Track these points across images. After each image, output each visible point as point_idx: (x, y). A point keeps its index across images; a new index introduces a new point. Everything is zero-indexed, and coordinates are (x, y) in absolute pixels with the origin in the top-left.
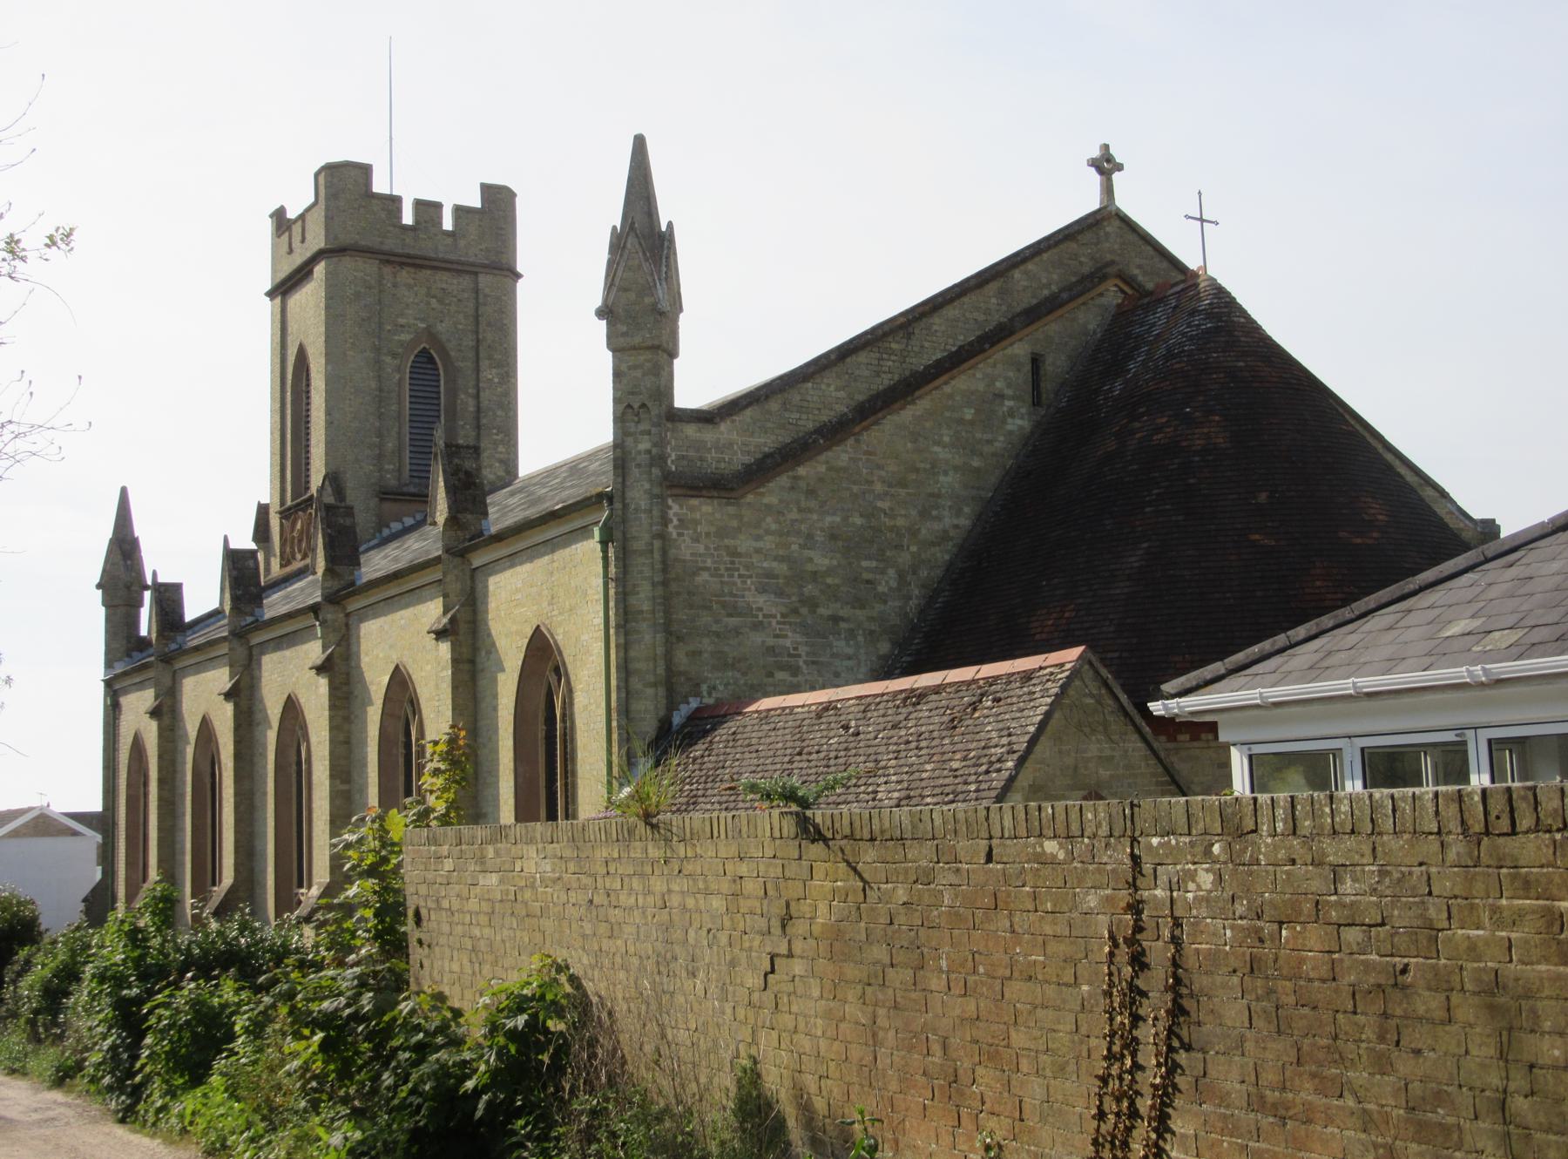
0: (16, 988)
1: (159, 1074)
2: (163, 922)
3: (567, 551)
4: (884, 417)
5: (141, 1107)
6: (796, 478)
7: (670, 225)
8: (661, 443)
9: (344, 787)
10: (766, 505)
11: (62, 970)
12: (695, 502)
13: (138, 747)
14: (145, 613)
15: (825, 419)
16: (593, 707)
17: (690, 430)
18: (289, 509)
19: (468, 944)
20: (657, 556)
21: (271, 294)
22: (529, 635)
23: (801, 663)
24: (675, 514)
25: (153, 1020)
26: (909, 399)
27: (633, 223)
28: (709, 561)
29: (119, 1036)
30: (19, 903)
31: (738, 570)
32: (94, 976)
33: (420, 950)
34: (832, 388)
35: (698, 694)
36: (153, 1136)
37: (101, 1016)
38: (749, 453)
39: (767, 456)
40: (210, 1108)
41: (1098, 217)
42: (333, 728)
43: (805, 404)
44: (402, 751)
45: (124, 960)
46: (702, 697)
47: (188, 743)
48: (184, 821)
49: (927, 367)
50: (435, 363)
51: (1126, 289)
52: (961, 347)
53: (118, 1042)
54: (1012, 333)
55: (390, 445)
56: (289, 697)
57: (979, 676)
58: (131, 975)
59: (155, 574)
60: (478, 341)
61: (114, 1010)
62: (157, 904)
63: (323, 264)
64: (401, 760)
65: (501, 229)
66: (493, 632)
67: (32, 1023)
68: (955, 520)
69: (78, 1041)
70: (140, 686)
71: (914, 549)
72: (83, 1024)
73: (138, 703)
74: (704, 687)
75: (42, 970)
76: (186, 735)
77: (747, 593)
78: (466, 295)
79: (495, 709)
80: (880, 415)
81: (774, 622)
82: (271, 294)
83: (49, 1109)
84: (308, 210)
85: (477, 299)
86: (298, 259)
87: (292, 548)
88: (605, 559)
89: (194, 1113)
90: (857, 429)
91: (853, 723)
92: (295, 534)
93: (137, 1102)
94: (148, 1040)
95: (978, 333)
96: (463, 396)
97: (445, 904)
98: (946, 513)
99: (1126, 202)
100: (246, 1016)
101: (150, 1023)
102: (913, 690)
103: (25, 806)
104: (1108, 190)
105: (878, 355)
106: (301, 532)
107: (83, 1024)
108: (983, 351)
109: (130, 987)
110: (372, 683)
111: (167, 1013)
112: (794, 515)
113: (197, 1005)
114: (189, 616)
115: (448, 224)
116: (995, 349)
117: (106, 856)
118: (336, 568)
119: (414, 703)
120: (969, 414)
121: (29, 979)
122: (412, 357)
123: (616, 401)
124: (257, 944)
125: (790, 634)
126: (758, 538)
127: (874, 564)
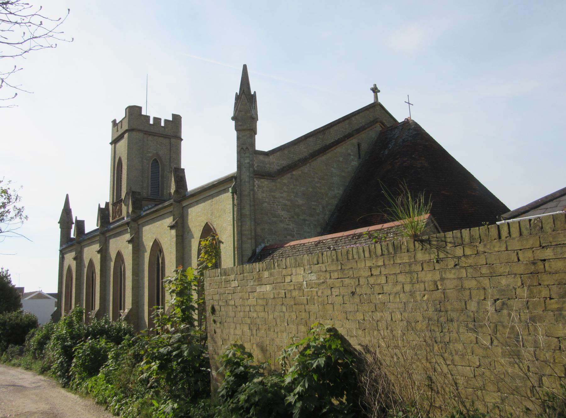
0: (29, 342)
1: (77, 372)
2: (80, 320)
3: (218, 198)
4: (318, 158)
5: (71, 383)
6: (293, 175)
7: (255, 92)
8: (252, 160)
9: (137, 278)
10: (284, 183)
11: (44, 336)
12: (262, 180)
13: (69, 269)
14: (72, 231)
15: (301, 157)
16: (228, 247)
17: (261, 157)
18: (115, 203)
19: (249, 321)
20: (252, 196)
21: (111, 143)
22: (203, 226)
23: (295, 234)
24: (257, 184)
25: (76, 353)
26: (325, 153)
27: (244, 91)
28: (267, 199)
29: (63, 358)
30: (31, 316)
31: (276, 203)
32: (55, 338)
33: (215, 325)
34: (303, 148)
35: (264, 242)
36: (75, 394)
37: (57, 351)
38: (279, 166)
39: (284, 167)
40: (98, 386)
41: (375, 104)
42: (134, 260)
43: (295, 152)
44: (156, 266)
45: (65, 333)
46: (265, 243)
47: (85, 267)
48: (83, 291)
49: (330, 144)
50: (158, 163)
51: (383, 126)
52: (339, 139)
53: (63, 360)
54: (353, 136)
55: (145, 185)
56: (118, 251)
57: (384, 227)
58: (68, 338)
59: (76, 218)
60: (170, 157)
61: (62, 349)
62: (77, 314)
63: (127, 134)
64: (156, 269)
65: (178, 126)
66: (190, 226)
67: (34, 353)
68: (338, 191)
69: (49, 358)
70: (71, 251)
71: (326, 199)
72: (51, 354)
73: (70, 257)
74: (266, 240)
75: (38, 336)
76: (85, 265)
77: (278, 210)
78: (167, 144)
79: (190, 250)
80: (317, 157)
81: (287, 220)
82: (111, 143)
83: (38, 382)
84: (123, 119)
85: (170, 145)
86: (120, 133)
87: (116, 214)
88: (233, 198)
89: (92, 387)
90: (310, 161)
91: (332, 247)
92: (117, 210)
93: (70, 381)
94: (74, 360)
95: (343, 135)
96: (166, 172)
97: (232, 303)
98: (335, 189)
99: (380, 100)
100: (113, 352)
101: (75, 354)
102: (355, 234)
103: (35, 291)
104: (376, 97)
105: (315, 139)
106: (119, 209)
107: (51, 354)
108: (345, 140)
109: (68, 342)
110: (146, 245)
111: (81, 351)
112: (292, 187)
113: (92, 348)
114: (86, 231)
115: (163, 124)
116: (349, 140)
117: (58, 304)
118: (136, 210)
119: (161, 251)
120: (341, 159)
121: (34, 339)
122: (152, 161)
123: (238, 146)
124: (110, 327)
125: (291, 224)
126: (282, 193)
127: (316, 203)
